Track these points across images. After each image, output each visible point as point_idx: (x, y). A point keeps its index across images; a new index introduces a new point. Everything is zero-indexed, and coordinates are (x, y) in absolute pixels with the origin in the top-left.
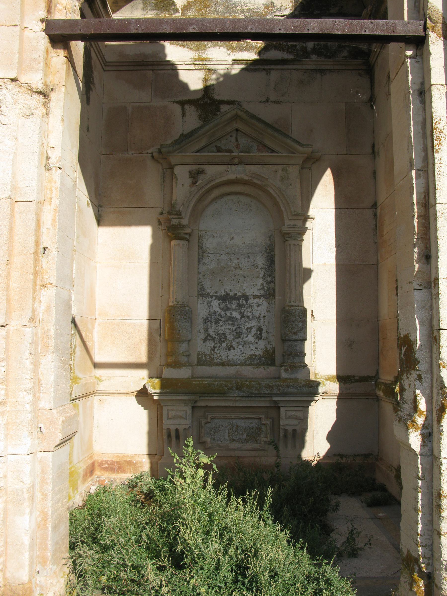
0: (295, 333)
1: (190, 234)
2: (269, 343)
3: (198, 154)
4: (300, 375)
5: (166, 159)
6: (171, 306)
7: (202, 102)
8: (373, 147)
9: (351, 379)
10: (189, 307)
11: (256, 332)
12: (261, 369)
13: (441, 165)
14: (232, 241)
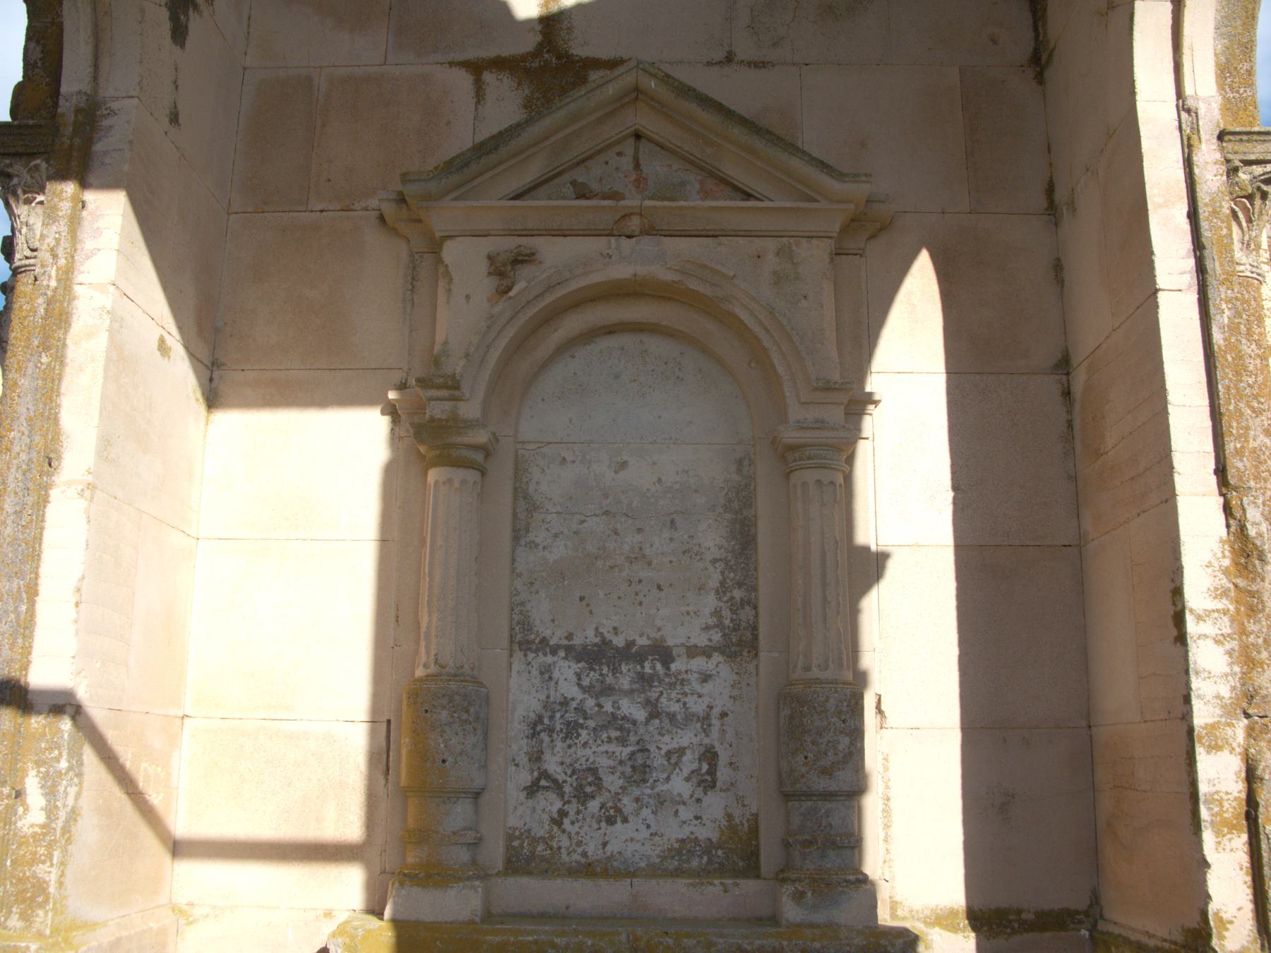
0: (827, 772)
1: (486, 451)
2: (740, 800)
3: (517, 203)
4: (845, 914)
5: (420, 221)
6: (421, 680)
7: (536, 65)
8: (1050, 190)
9: (1010, 922)
10: (481, 685)
11: (695, 766)
12: (714, 889)
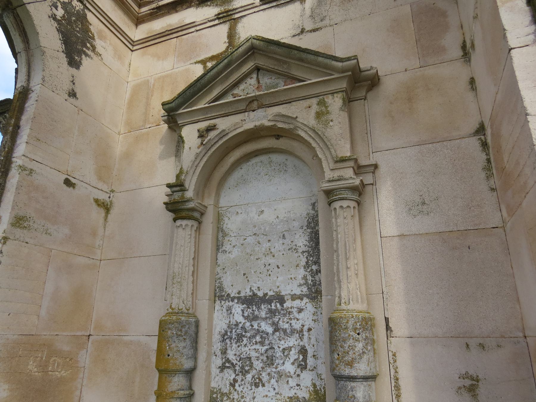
14: (261, 216)
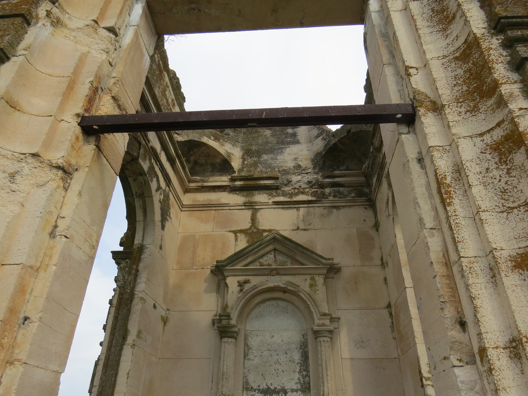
8: (382, 259)
13: (457, 217)
14: (273, 339)
